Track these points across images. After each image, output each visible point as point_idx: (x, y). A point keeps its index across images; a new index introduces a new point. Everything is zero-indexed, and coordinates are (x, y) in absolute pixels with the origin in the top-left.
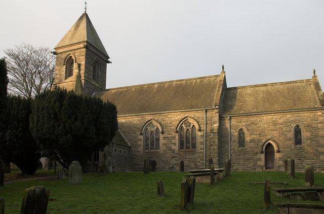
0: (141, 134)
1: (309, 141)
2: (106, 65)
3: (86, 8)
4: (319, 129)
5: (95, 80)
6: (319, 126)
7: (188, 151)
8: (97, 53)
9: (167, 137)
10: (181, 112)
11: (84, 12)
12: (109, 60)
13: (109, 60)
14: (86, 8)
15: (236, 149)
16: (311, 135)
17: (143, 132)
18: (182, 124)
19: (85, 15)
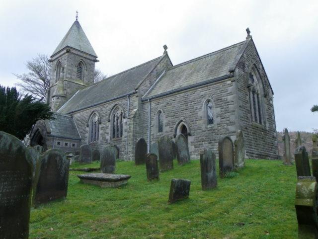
0: (88, 126)
1: (219, 118)
2: (94, 65)
3: (77, 17)
4: (229, 102)
5: (81, 79)
6: (230, 98)
7: (117, 140)
8: (81, 54)
9: (103, 127)
10: (201, 88)
11: (75, 20)
12: (97, 59)
13: (97, 59)
14: (77, 17)
15: (155, 135)
16: (222, 111)
17: (110, 118)
18: (114, 112)
19: (77, 23)
